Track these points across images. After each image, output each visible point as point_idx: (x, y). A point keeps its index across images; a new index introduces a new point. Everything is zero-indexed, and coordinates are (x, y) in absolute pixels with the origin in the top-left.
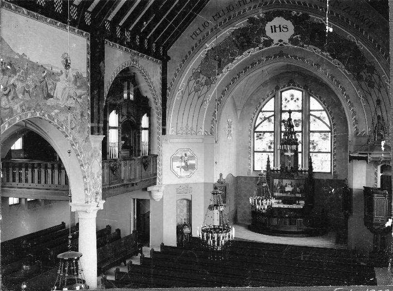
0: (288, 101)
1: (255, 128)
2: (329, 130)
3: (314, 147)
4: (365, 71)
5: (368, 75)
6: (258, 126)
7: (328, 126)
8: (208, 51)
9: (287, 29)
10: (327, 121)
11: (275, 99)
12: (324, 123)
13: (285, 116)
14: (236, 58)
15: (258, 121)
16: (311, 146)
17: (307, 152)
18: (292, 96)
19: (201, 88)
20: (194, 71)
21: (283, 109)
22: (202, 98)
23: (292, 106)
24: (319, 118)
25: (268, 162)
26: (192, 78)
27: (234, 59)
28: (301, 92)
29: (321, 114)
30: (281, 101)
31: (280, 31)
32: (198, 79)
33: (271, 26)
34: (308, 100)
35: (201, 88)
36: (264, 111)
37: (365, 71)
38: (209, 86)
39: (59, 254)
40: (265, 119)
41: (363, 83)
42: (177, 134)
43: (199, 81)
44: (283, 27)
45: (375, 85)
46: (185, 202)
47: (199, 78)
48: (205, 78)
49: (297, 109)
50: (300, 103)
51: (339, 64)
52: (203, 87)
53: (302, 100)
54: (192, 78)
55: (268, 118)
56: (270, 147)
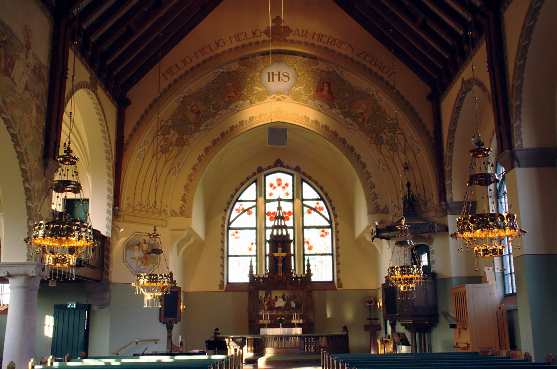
0: (275, 188)
1: (229, 224)
2: (327, 224)
3: (310, 248)
4: (386, 130)
5: (389, 135)
6: (233, 221)
7: (326, 219)
8: (184, 97)
9: (288, 77)
10: (325, 212)
11: (256, 185)
13: (272, 207)
14: (219, 113)
15: (234, 214)
16: (306, 246)
17: (302, 254)
18: (279, 180)
20: (163, 123)
21: (267, 198)
22: (170, 163)
23: (279, 193)
24: (315, 210)
25: (251, 267)
26: (160, 133)
27: (216, 114)
28: (291, 177)
29: (318, 204)
30: (265, 187)
31: (279, 80)
32: (167, 136)
33: (269, 74)
34: (300, 188)
35: (170, 149)
36: (241, 201)
37: (386, 130)
38: (180, 148)
39: (87, 221)
40: (244, 211)
41: (383, 147)
42: (134, 210)
43: (167, 138)
44: (283, 75)
45: (400, 148)
48: (177, 136)
49: (286, 198)
50: (290, 189)
51: (351, 125)
52: (173, 147)
53: (293, 186)
54: (160, 133)
55: (248, 210)
56: (250, 249)
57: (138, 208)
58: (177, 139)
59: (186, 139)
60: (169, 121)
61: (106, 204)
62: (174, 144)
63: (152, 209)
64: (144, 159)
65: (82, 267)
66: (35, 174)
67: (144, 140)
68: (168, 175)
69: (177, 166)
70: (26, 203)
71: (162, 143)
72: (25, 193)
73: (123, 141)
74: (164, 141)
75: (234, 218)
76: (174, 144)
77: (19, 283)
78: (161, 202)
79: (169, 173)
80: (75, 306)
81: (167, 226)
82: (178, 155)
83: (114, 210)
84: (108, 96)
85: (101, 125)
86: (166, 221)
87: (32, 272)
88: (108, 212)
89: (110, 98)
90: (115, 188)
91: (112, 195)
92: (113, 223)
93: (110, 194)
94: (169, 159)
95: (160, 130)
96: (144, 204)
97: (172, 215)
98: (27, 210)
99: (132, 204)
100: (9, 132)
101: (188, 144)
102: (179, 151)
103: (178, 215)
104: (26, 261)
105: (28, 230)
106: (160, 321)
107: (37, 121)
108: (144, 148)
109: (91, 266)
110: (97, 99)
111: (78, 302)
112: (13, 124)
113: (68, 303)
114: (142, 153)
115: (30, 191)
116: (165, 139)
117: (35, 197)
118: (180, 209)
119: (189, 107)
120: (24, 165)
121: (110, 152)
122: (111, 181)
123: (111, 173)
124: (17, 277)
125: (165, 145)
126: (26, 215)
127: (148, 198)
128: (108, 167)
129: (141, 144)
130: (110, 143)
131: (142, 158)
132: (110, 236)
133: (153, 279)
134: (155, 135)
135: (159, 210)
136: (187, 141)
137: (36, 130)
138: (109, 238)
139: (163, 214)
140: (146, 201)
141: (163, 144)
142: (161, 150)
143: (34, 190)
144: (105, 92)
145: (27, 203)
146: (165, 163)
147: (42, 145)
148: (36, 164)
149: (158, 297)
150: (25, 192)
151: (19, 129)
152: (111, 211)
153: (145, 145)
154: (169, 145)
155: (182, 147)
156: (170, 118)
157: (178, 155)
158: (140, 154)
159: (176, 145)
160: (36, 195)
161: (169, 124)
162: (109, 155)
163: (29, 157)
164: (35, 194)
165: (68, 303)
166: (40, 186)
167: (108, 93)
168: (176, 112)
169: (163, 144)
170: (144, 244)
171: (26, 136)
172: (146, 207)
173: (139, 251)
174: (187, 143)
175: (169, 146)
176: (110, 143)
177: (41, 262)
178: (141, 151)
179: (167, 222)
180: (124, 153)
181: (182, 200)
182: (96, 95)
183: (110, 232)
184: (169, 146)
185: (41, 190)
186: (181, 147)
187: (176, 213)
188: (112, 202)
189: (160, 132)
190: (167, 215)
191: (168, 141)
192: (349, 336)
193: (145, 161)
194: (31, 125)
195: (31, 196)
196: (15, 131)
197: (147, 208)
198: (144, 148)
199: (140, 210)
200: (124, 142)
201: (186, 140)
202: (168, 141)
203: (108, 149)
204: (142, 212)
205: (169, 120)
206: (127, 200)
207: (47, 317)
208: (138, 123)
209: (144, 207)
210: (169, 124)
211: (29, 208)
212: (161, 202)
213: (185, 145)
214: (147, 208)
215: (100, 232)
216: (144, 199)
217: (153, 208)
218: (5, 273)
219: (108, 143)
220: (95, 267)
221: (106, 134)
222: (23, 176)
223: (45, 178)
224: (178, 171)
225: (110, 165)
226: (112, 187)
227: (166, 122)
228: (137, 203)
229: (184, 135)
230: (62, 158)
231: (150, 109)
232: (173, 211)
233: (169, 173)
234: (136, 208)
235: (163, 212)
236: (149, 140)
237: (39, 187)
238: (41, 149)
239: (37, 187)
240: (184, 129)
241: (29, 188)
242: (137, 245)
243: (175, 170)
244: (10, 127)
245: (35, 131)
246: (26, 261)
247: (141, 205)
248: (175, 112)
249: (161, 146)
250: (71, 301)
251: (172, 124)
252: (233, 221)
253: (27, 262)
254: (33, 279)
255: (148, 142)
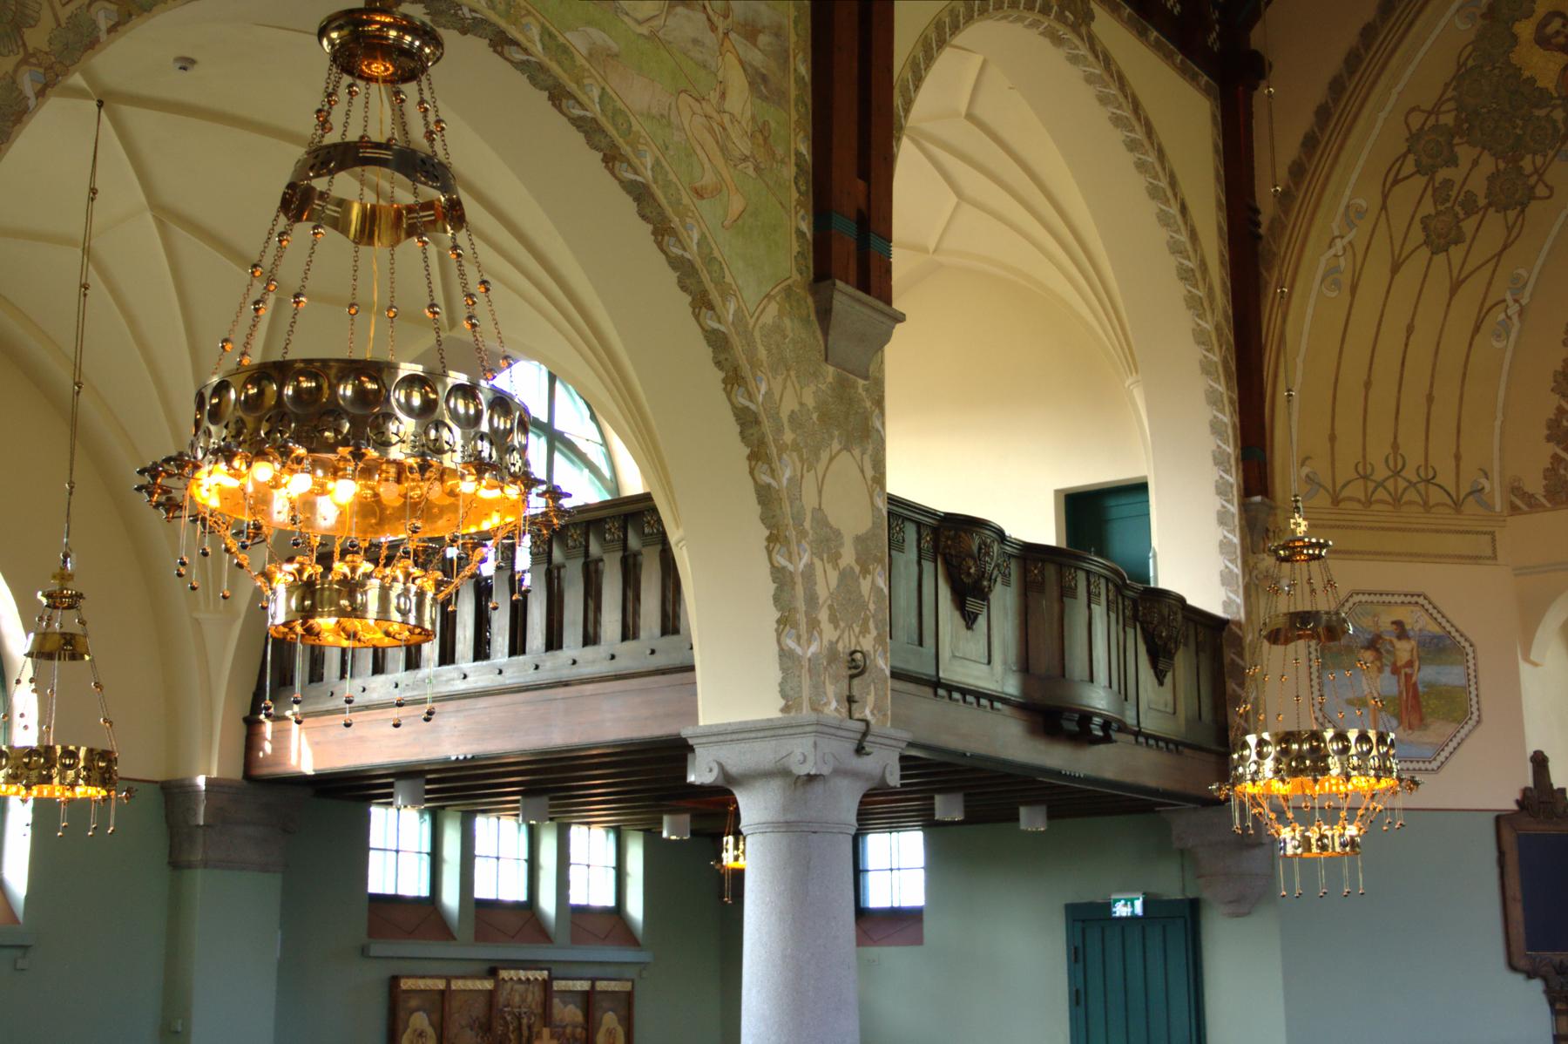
6: (1379, 215)
12: (1451, 271)
19: (1468, 225)
20: (1416, 121)
32: (1443, 174)
35: (1468, 225)
38: (1512, 214)
42: (1336, 501)
43: (1448, 183)
46: (1533, 657)
47: (1453, 161)
48: (1488, 164)
54: (1409, 166)
57: (1356, 490)
58: (1492, 179)
59: (1536, 171)
60: (1444, 108)
61: (1213, 489)
62: (1482, 202)
63: (1418, 492)
64: (1354, 289)
65: (1096, 741)
66: (769, 350)
67: (1341, 209)
68: (1472, 338)
69: (1508, 297)
70: (752, 472)
71: (1428, 208)
72: (741, 432)
73: (1258, 225)
74: (1433, 196)
75: (1488, 265)
76: (1482, 202)
77: (766, 808)
78: (1458, 457)
79: (1477, 329)
80: (1139, 909)
81: (1495, 557)
82: (1505, 248)
83: (1245, 507)
84: (1157, 47)
85: (1141, 166)
86: (1488, 538)
87: (801, 758)
88: (1222, 518)
89: (1168, 57)
90: (1242, 421)
91: (1230, 449)
92: (1252, 560)
93: (1224, 447)
94: (1469, 268)
95: (1409, 151)
96: (1381, 473)
97: (1514, 509)
98: (759, 503)
99: (1325, 478)
100: (621, 182)
101: (1545, 192)
102: (1510, 229)
103: (1543, 506)
104: (780, 715)
105: (776, 585)
106: (1513, 967)
107: (761, 133)
108: (1346, 240)
109: (1157, 739)
110: (1097, 57)
111: (1153, 889)
112: (620, 141)
113: (1114, 897)
114: (1342, 261)
115: (757, 422)
116: (1435, 190)
117: (782, 449)
118: (1545, 478)
119: (1525, 29)
120: (710, 313)
121: (1198, 275)
122: (1222, 394)
123: (1216, 358)
124: (758, 784)
125: (1438, 213)
126: (760, 522)
127: (1395, 446)
128: (1200, 338)
129: (1334, 225)
130: (1193, 236)
131: (1346, 280)
132: (1242, 616)
133: (1300, 757)
134: (1390, 179)
135: (1454, 496)
136: (1540, 179)
137: (757, 168)
138: (1238, 624)
139: (1470, 506)
140: (1387, 460)
141: (1433, 212)
142: (1428, 236)
143: (775, 417)
144: (1142, 34)
145: (756, 472)
146: (1453, 291)
147: (800, 234)
148: (773, 309)
149: (1343, 845)
150: (738, 429)
151: (657, 163)
152: (1233, 515)
153: (1351, 225)
154: (1458, 208)
155: (1523, 211)
156: (1444, 93)
157: (1505, 248)
158: (1332, 271)
159: (1490, 205)
160: (788, 437)
161: (1448, 119)
162: (1196, 286)
163: (728, 279)
164: (779, 430)
165: (1114, 897)
166: (810, 402)
167: (1154, 34)
168: (1470, 63)
169: (1433, 212)
170: (1399, 638)
171: (699, 193)
172: (1390, 484)
173: (1380, 670)
174: (1541, 191)
175: (1461, 215)
176: (1193, 236)
177: (851, 717)
178: (1336, 256)
179: (1494, 540)
180: (1265, 274)
181: (1549, 439)
182: (1091, 41)
183: (1240, 600)
184: (1461, 215)
185: (815, 416)
186: (1516, 212)
187: (1532, 496)
188: (1232, 479)
189: (1411, 158)
190: (1489, 507)
191: (1453, 194)
192: (1110, 745)
193: (1359, 291)
194: (724, 150)
195: (762, 442)
196: (636, 173)
197: (1396, 489)
198: (1346, 240)
199: (1363, 499)
200: (1262, 231)
201: (1535, 177)
202: (1453, 194)
203: (1186, 262)
204: (1376, 507)
205: (1440, 102)
206: (1303, 464)
207: (555, 988)
208: (1310, 143)
209: (1381, 484)
210: (1448, 119)
211: (765, 496)
212: (1458, 457)
213: (1534, 198)
214: (1396, 489)
215: (1181, 600)
216: (1378, 454)
217: (1421, 487)
218: (711, 770)
219: (1183, 238)
220: (1177, 744)
221: (1168, 200)
222: (718, 364)
223: (830, 370)
224: (1515, 319)
225: (1208, 326)
226: (1227, 418)
227: (1430, 113)
228: (1345, 472)
229: (1522, 158)
230: (339, 28)
231: (1352, 73)
232: (1517, 490)
233: (1477, 329)
234: (1345, 493)
235: (1471, 498)
236: (1364, 204)
237: (802, 404)
238: (796, 248)
239: (788, 405)
240: (1519, 131)
241: (747, 408)
242: (1367, 648)
243: (1502, 316)
244: (614, 158)
245: (751, 171)
246: (780, 715)
247: (1365, 477)
248: (1465, 64)
249: (1422, 221)
250: (1122, 890)
251: (1457, 118)
252: (1379, 215)
253: (780, 719)
254: (818, 788)
255: (1361, 213)
